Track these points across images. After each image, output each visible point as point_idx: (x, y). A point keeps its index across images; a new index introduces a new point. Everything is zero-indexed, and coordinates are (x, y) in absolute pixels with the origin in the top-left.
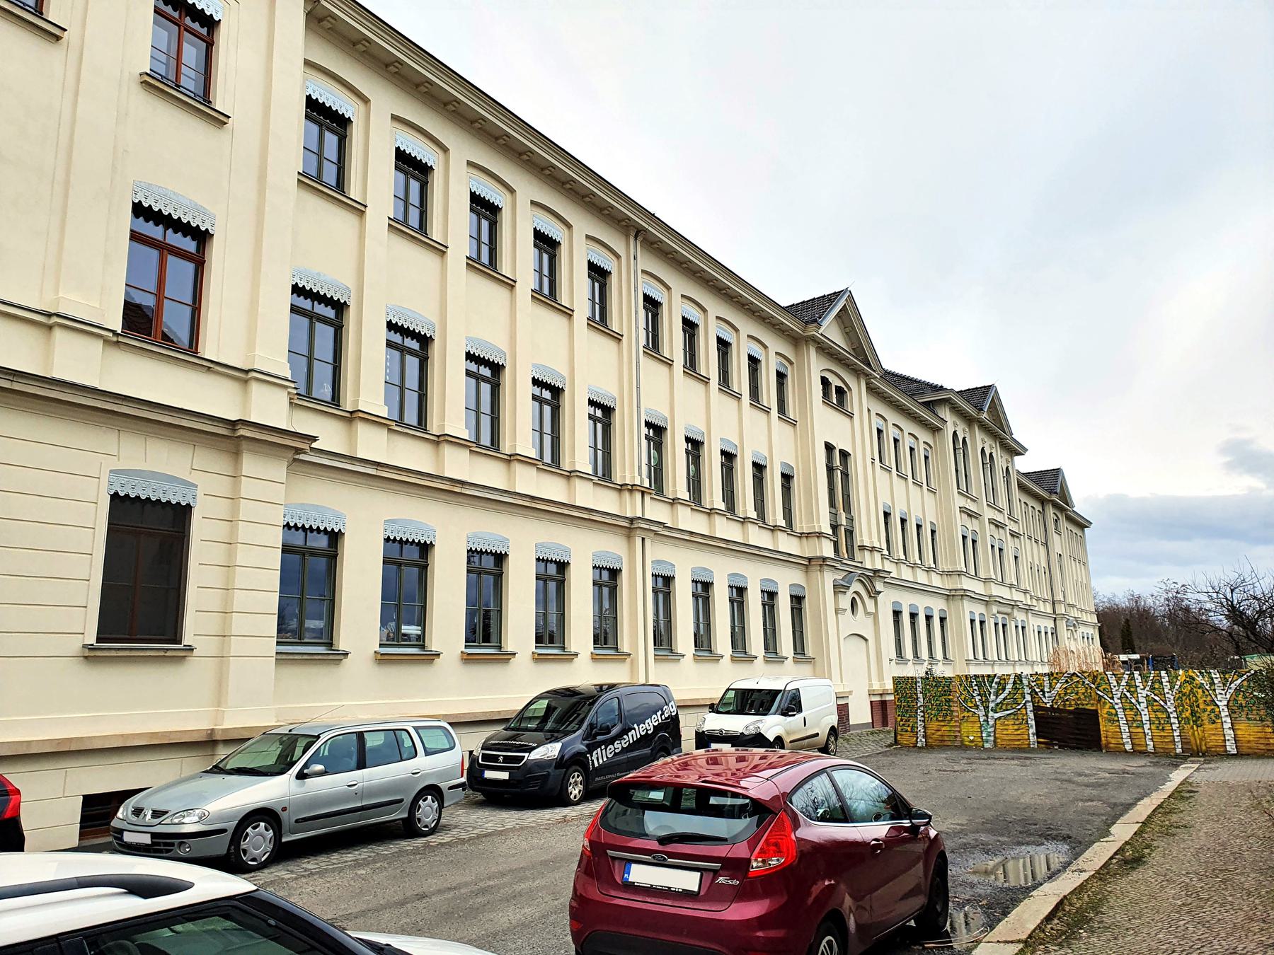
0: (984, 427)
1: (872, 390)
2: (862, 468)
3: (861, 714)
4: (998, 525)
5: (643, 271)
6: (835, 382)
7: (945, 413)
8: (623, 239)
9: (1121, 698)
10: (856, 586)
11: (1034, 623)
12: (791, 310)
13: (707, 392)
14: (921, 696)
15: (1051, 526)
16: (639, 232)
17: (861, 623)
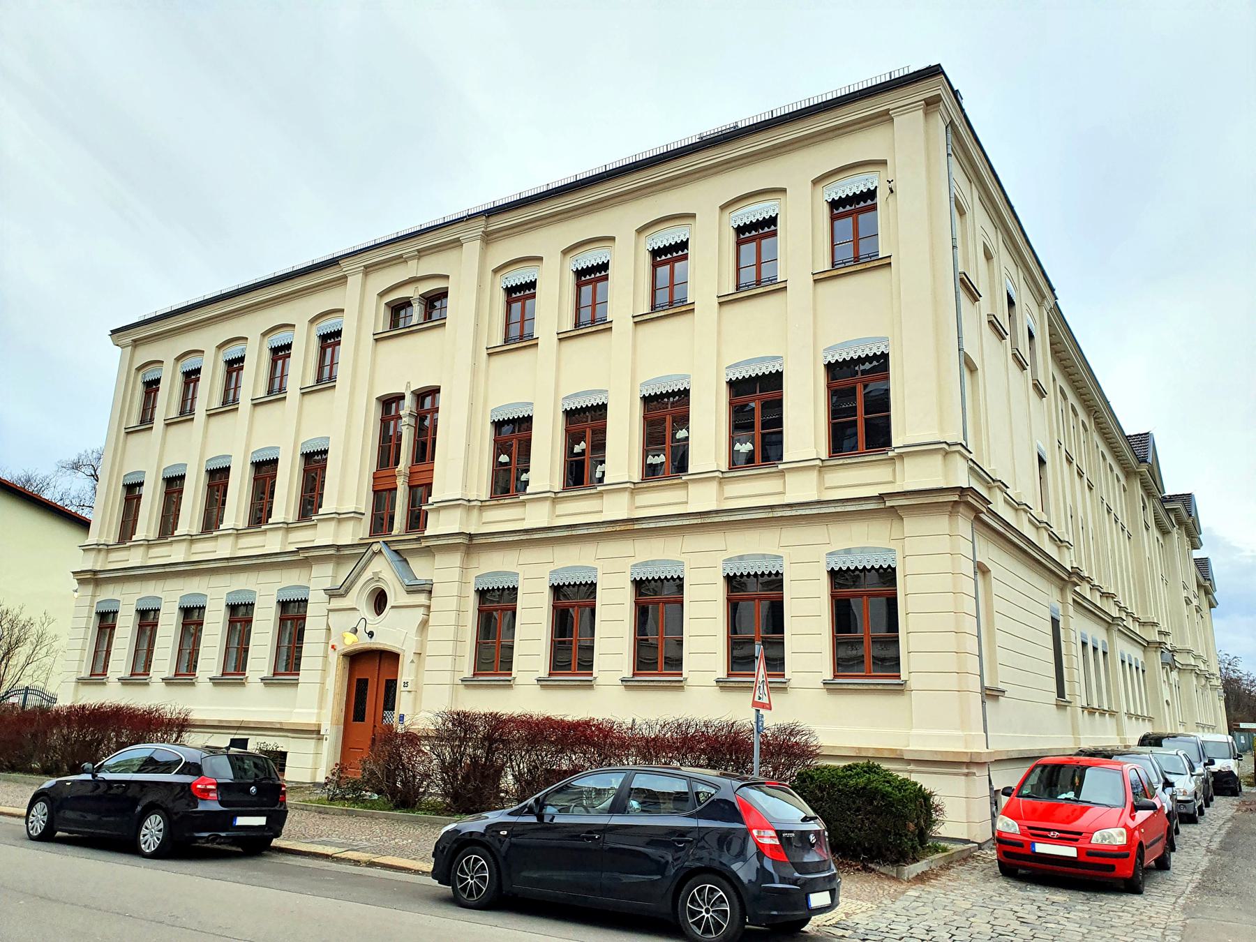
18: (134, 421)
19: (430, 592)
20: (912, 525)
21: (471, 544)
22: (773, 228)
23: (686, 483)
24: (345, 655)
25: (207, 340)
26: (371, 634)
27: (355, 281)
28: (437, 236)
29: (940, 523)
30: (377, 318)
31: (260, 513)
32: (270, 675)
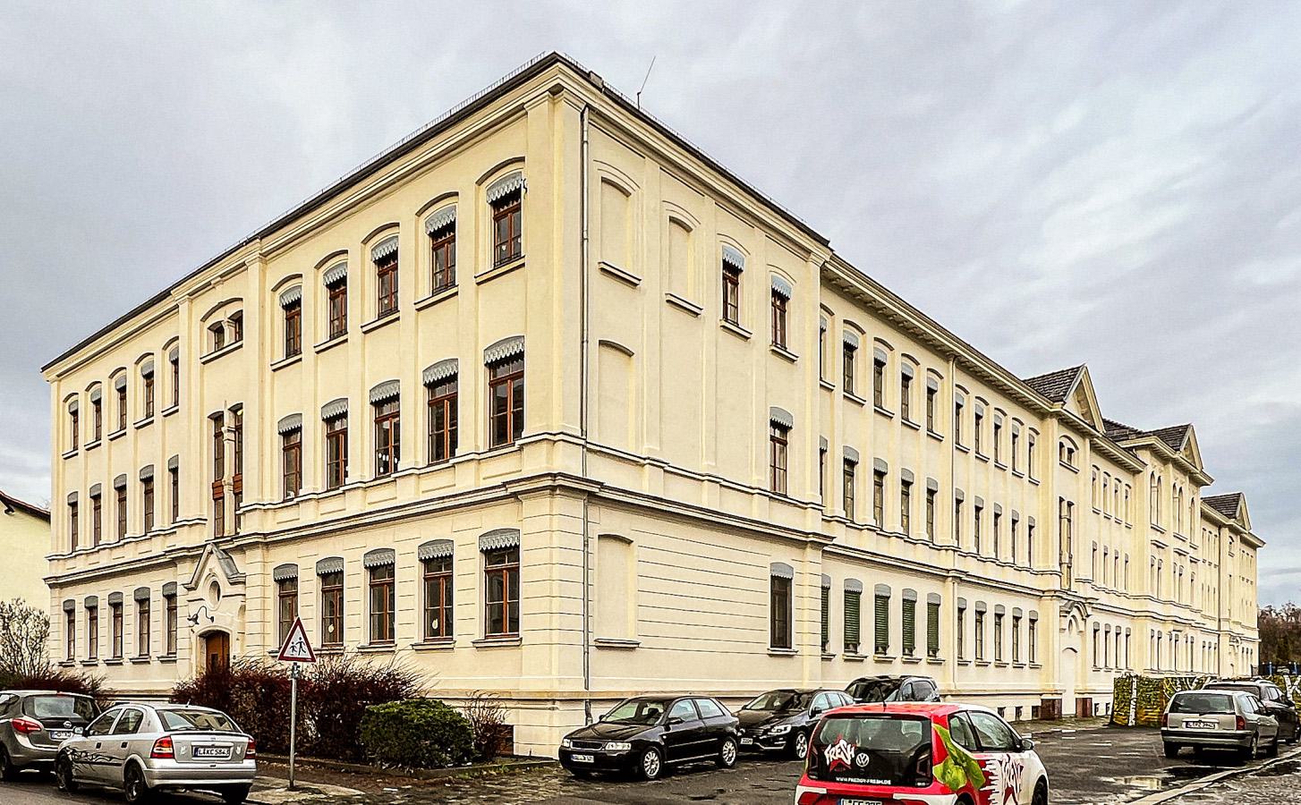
0: (1178, 466)
1: (1095, 449)
2: (1081, 514)
3: (1027, 715)
4: (1180, 553)
5: (957, 385)
6: (1068, 445)
7: (1145, 456)
8: (945, 364)
9: (1293, 694)
10: (1075, 612)
11: (1200, 638)
12: (1030, 383)
13: (832, 400)
14: (1135, 691)
15: (1225, 549)
16: (632, 137)
17: (1073, 639)
18: (280, 354)
19: (244, 583)
20: (531, 506)
21: (267, 542)
22: (298, 309)
23: (521, 448)
24: (200, 636)
25: (126, 356)
26: (212, 619)
27: (254, 269)
28: (227, 264)
29: (561, 503)
30: (207, 343)
31: (443, 445)
32: (165, 654)
